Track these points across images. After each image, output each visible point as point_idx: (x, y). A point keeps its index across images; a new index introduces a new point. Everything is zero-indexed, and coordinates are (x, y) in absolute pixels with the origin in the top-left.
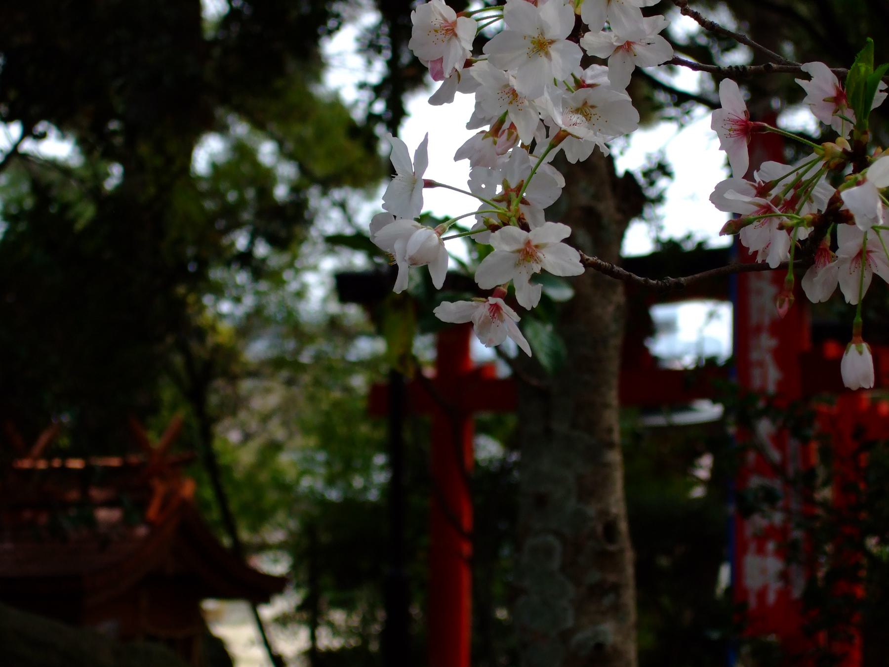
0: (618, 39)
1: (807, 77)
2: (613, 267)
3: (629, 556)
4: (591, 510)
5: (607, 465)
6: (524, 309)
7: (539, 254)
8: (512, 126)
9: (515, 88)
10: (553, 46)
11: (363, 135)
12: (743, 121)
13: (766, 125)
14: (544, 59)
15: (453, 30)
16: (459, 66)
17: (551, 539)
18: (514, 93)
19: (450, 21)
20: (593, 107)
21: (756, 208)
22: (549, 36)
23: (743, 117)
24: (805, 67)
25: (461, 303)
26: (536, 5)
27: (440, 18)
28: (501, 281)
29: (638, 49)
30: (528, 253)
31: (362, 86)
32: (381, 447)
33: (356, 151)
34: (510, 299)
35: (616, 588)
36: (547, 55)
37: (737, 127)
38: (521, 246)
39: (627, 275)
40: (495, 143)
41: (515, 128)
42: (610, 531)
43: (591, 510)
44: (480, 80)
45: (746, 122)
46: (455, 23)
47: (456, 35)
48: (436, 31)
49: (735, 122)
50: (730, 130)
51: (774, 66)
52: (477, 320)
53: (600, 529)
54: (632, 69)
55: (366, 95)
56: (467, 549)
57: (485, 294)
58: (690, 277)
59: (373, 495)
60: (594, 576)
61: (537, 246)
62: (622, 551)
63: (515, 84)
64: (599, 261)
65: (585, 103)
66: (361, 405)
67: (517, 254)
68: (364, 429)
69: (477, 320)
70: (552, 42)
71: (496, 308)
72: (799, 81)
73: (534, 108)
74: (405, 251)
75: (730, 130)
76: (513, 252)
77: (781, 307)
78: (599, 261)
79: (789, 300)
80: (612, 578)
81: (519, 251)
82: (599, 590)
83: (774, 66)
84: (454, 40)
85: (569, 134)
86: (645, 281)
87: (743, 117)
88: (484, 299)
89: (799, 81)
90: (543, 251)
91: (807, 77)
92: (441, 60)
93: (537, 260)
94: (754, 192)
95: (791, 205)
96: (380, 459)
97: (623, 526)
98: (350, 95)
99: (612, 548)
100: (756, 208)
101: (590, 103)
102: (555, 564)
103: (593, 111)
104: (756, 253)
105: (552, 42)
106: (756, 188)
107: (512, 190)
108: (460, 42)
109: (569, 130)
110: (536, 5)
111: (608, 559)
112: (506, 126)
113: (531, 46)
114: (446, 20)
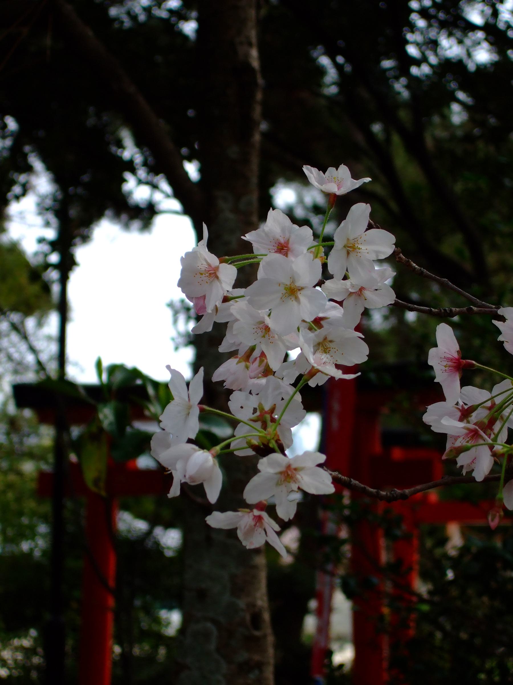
0: (353, 286)
1: (502, 319)
2: (351, 481)
3: (271, 639)
4: (242, 603)
5: (255, 567)
6: (282, 520)
7: (298, 476)
8: (263, 355)
9: (270, 326)
10: (302, 292)
11: (36, 274)
12: (456, 359)
13: (474, 362)
14: (295, 303)
15: (215, 273)
16: (219, 303)
17: (209, 625)
18: (267, 329)
19: (213, 266)
20: (331, 341)
21: (466, 431)
22: (299, 284)
23: (456, 355)
24: (500, 312)
25: (230, 513)
26: (287, 256)
27: (204, 263)
28: (264, 498)
29: (367, 294)
30: (288, 475)
31: (41, 241)
32: (45, 518)
33: (34, 289)
34: (271, 510)
35: (260, 666)
36: (297, 299)
37: (450, 363)
38: (283, 469)
39: (362, 488)
40: (247, 367)
41: (265, 356)
42: (256, 620)
43: (242, 603)
44: (238, 317)
45: (458, 360)
46: (217, 268)
47: (217, 277)
48: (201, 274)
49: (451, 360)
50: (445, 366)
51: (475, 309)
52: (243, 527)
53: (248, 617)
54: (362, 310)
55: (46, 248)
56: (111, 602)
57: (250, 507)
58: (413, 489)
59: (37, 553)
60: (243, 656)
61: (295, 469)
62: (265, 636)
63: (269, 321)
64: (340, 476)
65: (325, 339)
66: (32, 485)
67: (279, 475)
68: (31, 504)
69: (243, 527)
70: (301, 289)
71: (259, 519)
72: (495, 322)
73: (283, 341)
74: (185, 471)
75: (445, 366)
76: (276, 474)
77: (492, 520)
78: (340, 476)
79: (500, 516)
80: (257, 657)
81: (281, 473)
82: (246, 667)
83: (475, 309)
84: (216, 283)
85: (319, 371)
86: (377, 492)
87: (456, 355)
88: (248, 510)
89: (495, 322)
90: (301, 473)
91: (502, 319)
92: (204, 297)
93: (296, 481)
94: (459, 414)
95: (488, 426)
96: (43, 528)
97: (266, 616)
98: (30, 247)
99: (257, 633)
100: (466, 431)
101: (329, 338)
102: (212, 646)
103: (331, 345)
104: (462, 467)
105: (301, 289)
106: (460, 411)
107: (266, 413)
108: (221, 283)
109: (320, 368)
110: (287, 256)
111: (254, 643)
112: (256, 353)
113: (284, 291)
114: (209, 265)
